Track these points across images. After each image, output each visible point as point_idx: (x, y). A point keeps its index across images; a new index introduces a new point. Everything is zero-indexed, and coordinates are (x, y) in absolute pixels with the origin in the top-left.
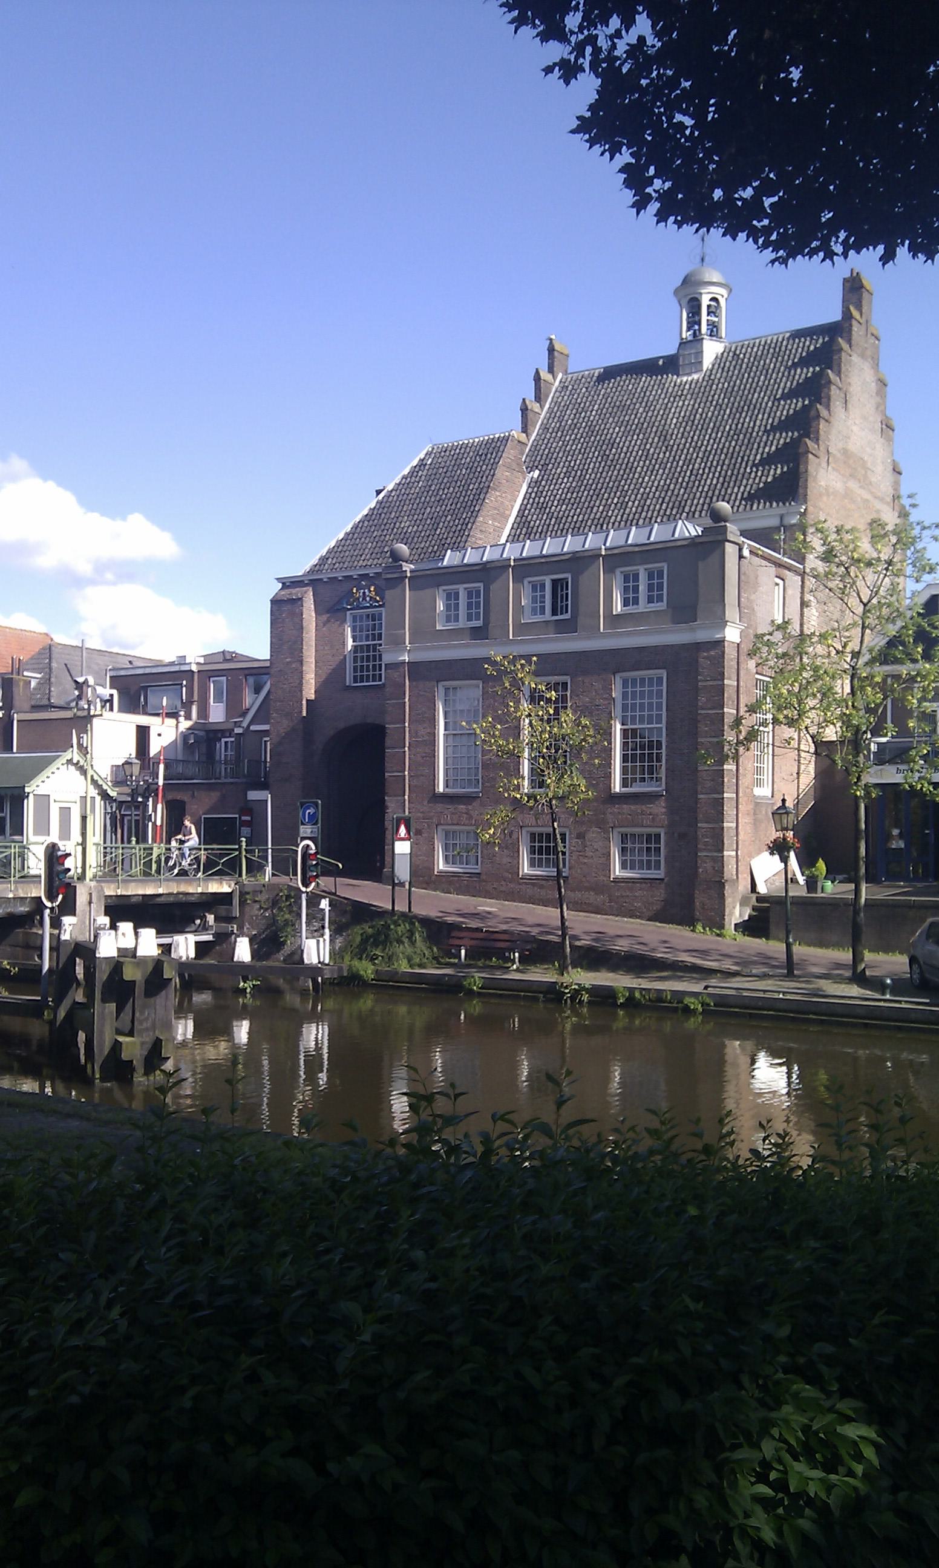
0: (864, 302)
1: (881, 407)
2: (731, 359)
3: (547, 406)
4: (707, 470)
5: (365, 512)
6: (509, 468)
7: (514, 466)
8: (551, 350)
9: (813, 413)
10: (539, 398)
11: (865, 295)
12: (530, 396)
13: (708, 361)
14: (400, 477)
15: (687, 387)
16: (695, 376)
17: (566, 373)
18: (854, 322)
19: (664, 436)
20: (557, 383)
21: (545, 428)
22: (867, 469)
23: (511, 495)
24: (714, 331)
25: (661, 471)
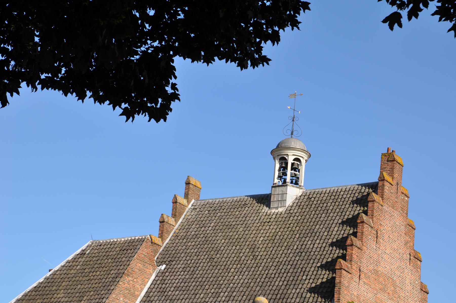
0: (395, 171)
1: (410, 243)
2: (306, 201)
3: (181, 220)
4: (277, 275)
5: (35, 285)
7: (147, 260)
8: (188, 183)
9: (349, 242)
10: (175, 215)
11: (397, 166)
12: (168, 212)
13: (289, 202)
14: (66, 261)
15: (274, 216)
16: (280, 210)
17: (197, 200)
18: (386, 183)
19: (253, 249)
20: (190, 206)
21: (176, 236)
22: (395, 286)
25: (247, 273)
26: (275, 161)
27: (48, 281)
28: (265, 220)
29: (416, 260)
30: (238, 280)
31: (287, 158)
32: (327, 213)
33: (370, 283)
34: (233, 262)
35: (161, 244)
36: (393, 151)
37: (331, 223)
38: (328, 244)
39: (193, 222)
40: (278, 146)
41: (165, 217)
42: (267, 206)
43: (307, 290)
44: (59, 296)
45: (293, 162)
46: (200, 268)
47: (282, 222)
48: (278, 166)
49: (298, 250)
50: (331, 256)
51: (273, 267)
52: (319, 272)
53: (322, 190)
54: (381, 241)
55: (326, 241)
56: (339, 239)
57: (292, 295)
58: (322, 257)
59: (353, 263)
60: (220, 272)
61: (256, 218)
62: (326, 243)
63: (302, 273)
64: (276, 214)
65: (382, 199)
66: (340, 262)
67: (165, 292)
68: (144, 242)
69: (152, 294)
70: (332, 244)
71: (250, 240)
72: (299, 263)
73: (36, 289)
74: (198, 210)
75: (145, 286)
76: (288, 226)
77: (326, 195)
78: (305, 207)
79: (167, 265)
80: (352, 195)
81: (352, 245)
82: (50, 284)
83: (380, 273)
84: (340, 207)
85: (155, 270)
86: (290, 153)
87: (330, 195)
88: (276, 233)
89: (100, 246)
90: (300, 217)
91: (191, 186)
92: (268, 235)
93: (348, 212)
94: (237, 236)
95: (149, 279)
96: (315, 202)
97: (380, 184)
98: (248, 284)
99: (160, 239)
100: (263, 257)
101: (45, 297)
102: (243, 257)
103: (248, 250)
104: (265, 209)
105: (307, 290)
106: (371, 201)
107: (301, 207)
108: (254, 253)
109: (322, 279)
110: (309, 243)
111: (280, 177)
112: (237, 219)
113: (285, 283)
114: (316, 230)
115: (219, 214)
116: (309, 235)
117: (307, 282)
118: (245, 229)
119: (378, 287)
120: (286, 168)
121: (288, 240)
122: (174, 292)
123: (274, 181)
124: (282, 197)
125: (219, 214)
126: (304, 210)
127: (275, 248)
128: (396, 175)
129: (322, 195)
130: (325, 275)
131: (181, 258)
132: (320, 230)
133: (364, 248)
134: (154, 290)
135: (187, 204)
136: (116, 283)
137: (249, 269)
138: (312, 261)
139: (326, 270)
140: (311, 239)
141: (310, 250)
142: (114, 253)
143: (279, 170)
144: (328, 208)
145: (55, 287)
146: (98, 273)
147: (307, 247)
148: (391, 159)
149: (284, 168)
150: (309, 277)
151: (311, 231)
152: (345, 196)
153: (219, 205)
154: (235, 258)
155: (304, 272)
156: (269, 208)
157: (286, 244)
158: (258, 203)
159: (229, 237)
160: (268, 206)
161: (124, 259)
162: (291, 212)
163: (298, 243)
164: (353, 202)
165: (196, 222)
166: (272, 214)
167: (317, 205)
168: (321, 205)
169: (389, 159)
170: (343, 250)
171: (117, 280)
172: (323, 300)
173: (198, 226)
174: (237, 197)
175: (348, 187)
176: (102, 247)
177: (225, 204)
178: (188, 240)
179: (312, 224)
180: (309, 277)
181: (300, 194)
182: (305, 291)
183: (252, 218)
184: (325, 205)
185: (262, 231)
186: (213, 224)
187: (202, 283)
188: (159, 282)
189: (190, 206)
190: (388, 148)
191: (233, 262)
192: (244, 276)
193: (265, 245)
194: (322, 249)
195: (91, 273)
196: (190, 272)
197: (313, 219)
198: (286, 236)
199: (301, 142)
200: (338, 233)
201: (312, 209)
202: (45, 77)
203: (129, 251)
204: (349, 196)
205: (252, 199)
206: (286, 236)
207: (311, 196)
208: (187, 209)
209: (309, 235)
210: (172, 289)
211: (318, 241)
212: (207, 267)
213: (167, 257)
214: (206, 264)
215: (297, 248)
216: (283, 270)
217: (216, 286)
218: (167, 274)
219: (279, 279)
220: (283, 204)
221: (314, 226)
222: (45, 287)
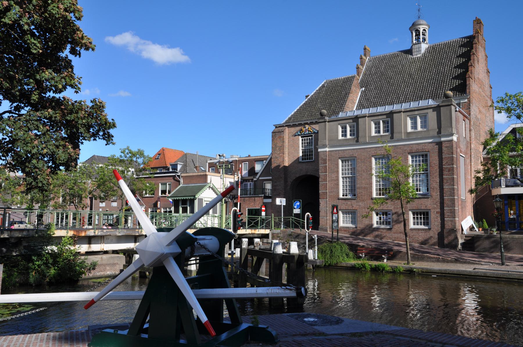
2: (432, 50)
8: (365, 49)
13: (423, 51)
16: (419, 55)
17: (369, 56)
19: (410, 75)
21: (365, 74)
23: (356, 96)
48: (414, 34)
52: (453, 81)
70: (455, 67)
86: (421, 27)
97: (477, 35)
104: (410, 56)
120: (419, 35)
123: (413, 42)
149: (418, 35)
160: (412, 54)
169: (478, 22)
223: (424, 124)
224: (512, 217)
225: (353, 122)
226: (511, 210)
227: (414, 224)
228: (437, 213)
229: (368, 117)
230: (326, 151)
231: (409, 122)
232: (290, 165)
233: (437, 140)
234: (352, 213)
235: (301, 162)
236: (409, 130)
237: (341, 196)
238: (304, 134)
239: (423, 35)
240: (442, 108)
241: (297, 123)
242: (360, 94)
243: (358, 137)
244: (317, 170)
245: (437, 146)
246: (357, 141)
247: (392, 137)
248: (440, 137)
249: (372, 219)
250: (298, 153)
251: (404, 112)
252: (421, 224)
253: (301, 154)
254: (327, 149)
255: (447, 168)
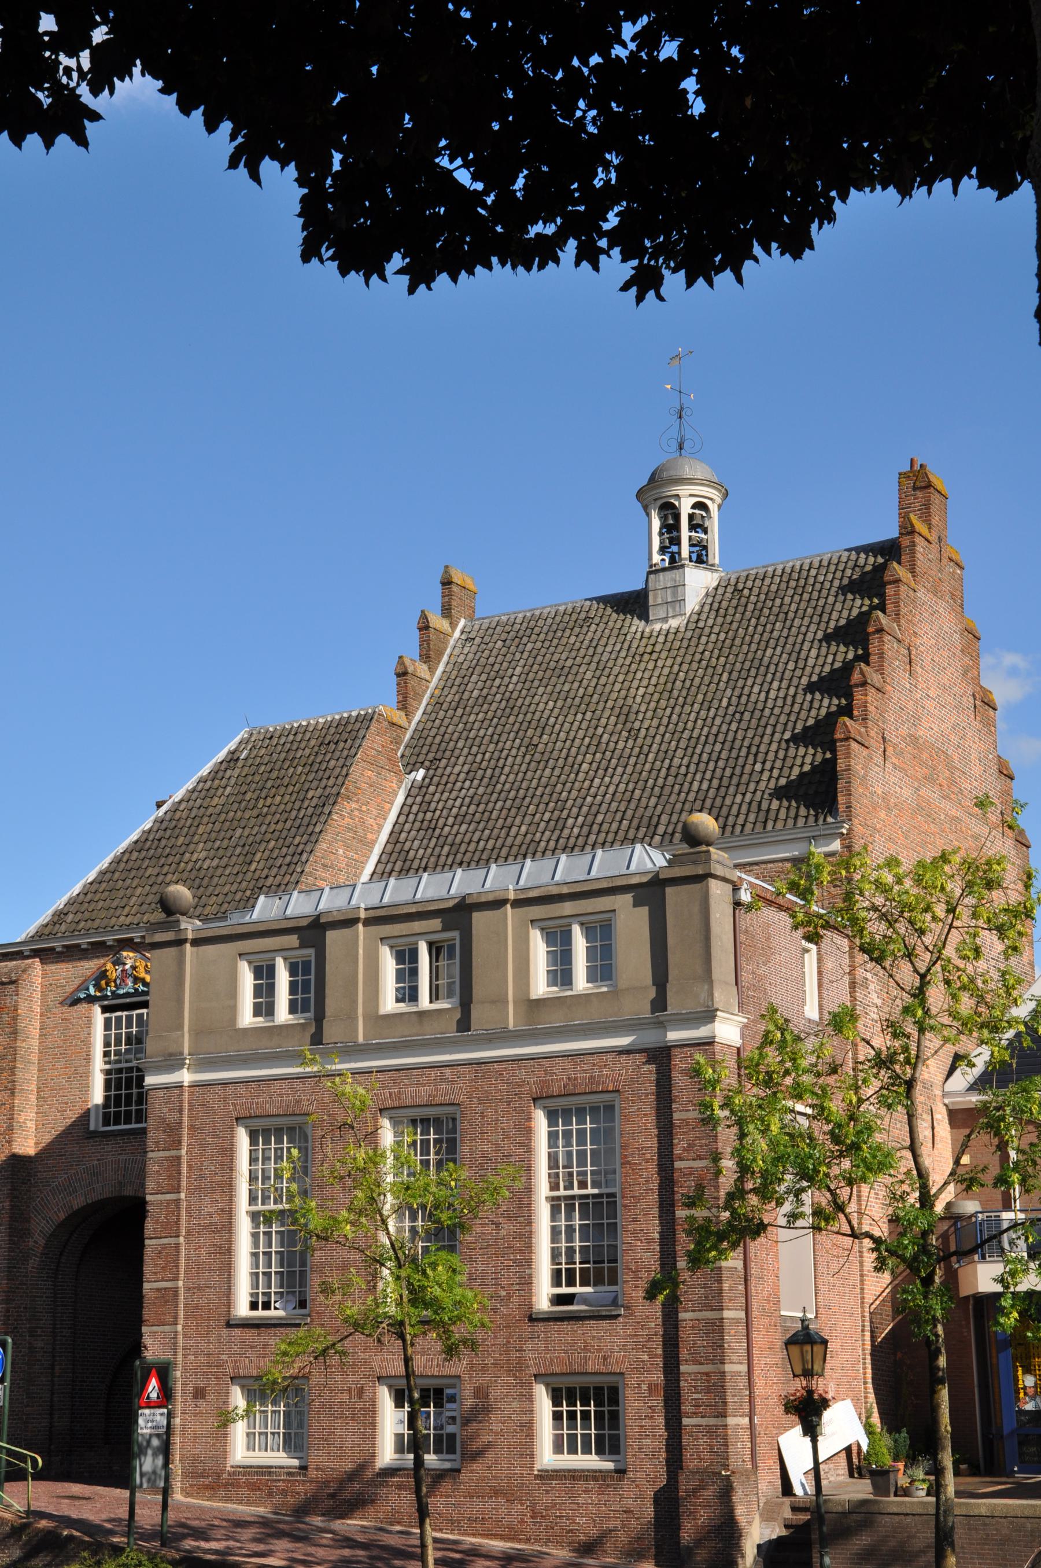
0: (934, 509)
1: (971, 673)
2: (732, 598)
3: (441, 668)
4: (692, 768)
5: (134, 836)
6: (373, 763)
7: (383, 761)
8: (447, 582)
9: (856, 677)
10: (428, 656)
11: (936, 499)
12: (411, 651)
13: (692, 602)
15: (661, 639)
16: (674, 623)
17: (471, 618)
18: (918, 540)
19: (625, 715)
20: (457, 634)
21: (437, 703)
22: (951, 768)
23: (377, 805)
24: (701, 558)
25: (620, 770)
26: (648, 515)
27: (163, 826)
28: (641, 650)
29: (987, 707)
30: (603, 788)
31: (677, 503)
32: (786, 619)
33: (905, 767)
34: (583, 749)
35: (406, 725)
36: (921, 466)
37: (799, 640)
38: (801, 687)
39: (471, 670)
40: (652, 479)
41: (407, 662)
42: (640, 618)
43: (770, 794)
44: (195, 856)
45: (691, 511)
46: (507, 769)
47: (683, 651)
48: (656, 524)
49: (731, 709)
50: (813, 713)
51: (679, 750)
52: (792, 752)
53: (764, 570)
54: (919, 670)
55: (795, 681)
56: (824, 674)
57: (735, 808)
58: (793, 718)
59: (870, 724)
60: (557, 772)
61: (618, 647)
62: (797, 687)
63: (751, 758)
64: (664, 633)
65: (913, 576)
66: (844, 724)
67: (434, 829)
68: (374, 721)
69: (404, 835)
70: (811, 688)
71: (614, 696)
72: (740, 736)
73: (138, 846)
74: (478, 640)
75: (385, 819)
76: (698, 657)
77: (777, 580)
78: (731, 611)
79: (428, 769)
80: (839, 575)
81: (864, 684)
82: (169, 832)
83: (921, 741)
84: (813, 603)
85: (402, 782)
86: (683, 490)
87: (785, 579)
88: (672, 677)
89: (271, 738)
90: (722, 636)
91: (455, 588)
92: (654, 681)
93: (834, 613)
94: (581, 690)
95: (392, 803)
96: (753, 599)
97: (905, 541)
98: (628, 794)
99: (403, 714)
100: (652, 731)
101: (162, 861)
102: (606, 737)
103: (613, 719)
104: (638, 625)
105: (770, 794)
106: (890, 583)
107: (722, 611)
108: (628, 725)
109: (802, 766)
110: (756, 689)
111: (663, 550)
112: (574, 654)
113: (715, 783)
114: (766, 660)
115: (530, 646)
116: (753, 672)
117: (766, 775)
118: (598, 673)
119: (921, 772)
120: (676, 527)
121: (704, 688)
122: (456, 827)
123: (650, 558)
124: (675, 594)
125: (530, 646)
126: (729, 619)
127: (678, 709)
128: (935, 520)
129: (767, 581)
130: (807, 758)
131: (457, 752)
132: (775, 659)
133: (888, 688)
134: (407, 826)
135: (450, 630)
136: (323, 818)
137: (623, 761)
138: (769, 730)
139: (806, 747)
140: (759, 680)
141: (760, 706)
142: (307, 751)
143: (661, 534)
144: (785, 608)
145: (181, 839)
146: (278, 798)
147: (753, 698)
148: (923, 484)
149: (671, 528)
150: (768, 765)
151: (756, 663)
152: (821, 578)
153: (525, 625)
154: (587, 740)
155: (756, 755)
156: (647, 621)
157: (700, 697)
158: (617, 612)
159: (563, 695)
160: (644, 616)
161: (332, 763)
162: (701, 624)
163: (729, 692)
164: (843, 590)
165: (478, 669)
166: (655, 634)
167: (760, 605)
168: (769, 603)
169: (917, 483)
170: (839, 698)
171: (326, 810)
172: (812, 812)
173: (484, 677)
174: (565, 604)
175: (826, 558)
176: (275, 741)
177: (541, 623)
178: (468, 709)
179: (754, 647)
180: (768, 765)
181: (715, 584)
182: (766, 796)
183: (609, 648)
184: (778, 602)
185: (639, 675)
186: (518, 670)
187: (518, 801)
188: (415, 808)
189: (457, 634)
190: (912, 460)
191: (583, 749)
192: (615, 777)
193: (653, 705)
194: (789, 701)
195: (262, 802)
196: (486, 781)
197: (756, 636)
198: (697, 680)
199: (704, 465)
200: (820, 661)
201: (748, 614)
202: (616, 215)
203: (341, 745)
204: (830, 577)
205: (602, 606)
206: (697, 680)
207: (740, 586)
208: (452, 642)
209: (753, 672)
210: (451, 820)
211: (775, 685)
212: (524, 766)
213: (424, 751)
214: (519, 759)
215: (729, 704)
216: (705, 757)
217: (552, 805)
218: (432, 789)
219: (698, 777)
220: (677, 609)
221: (759, 652)
222: (159, 840)
223: (602, 967)
224: (1029, 1407)
225: (302, 946)
226: (1027, 1371)
227: (558, 1449)
228: (652, 1389)
229: (368, 922)
230: (179, 1086)
231: (539, 949)
232: (46, 1153)
233: (650, 1038)
234: (290, 1399)
235: (95, 1134)
236: (540, 987)
237: (242, 1309)
238: (115, 995)
239: (693, 527)
240: (669, 890)
241: (83, 942)
242: (400, 799)
243: (319, 1018)
244: (141, 1175)
245: (652, 1068)
246: (317, 1039)
247: (464, 1024)
248: (662, 1026)
249: (373, 1424)
250: (86, 1088)
251: (517, 903)
252: (587, 1451)
253: (97, 1096)
254: (186, 1077)
255: (691, 1171)
